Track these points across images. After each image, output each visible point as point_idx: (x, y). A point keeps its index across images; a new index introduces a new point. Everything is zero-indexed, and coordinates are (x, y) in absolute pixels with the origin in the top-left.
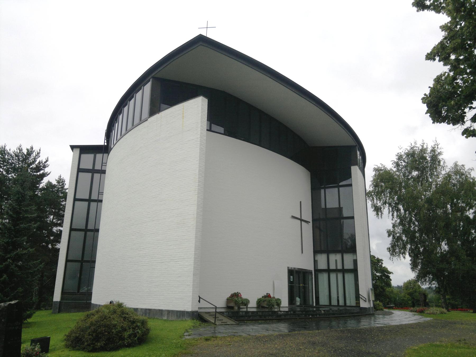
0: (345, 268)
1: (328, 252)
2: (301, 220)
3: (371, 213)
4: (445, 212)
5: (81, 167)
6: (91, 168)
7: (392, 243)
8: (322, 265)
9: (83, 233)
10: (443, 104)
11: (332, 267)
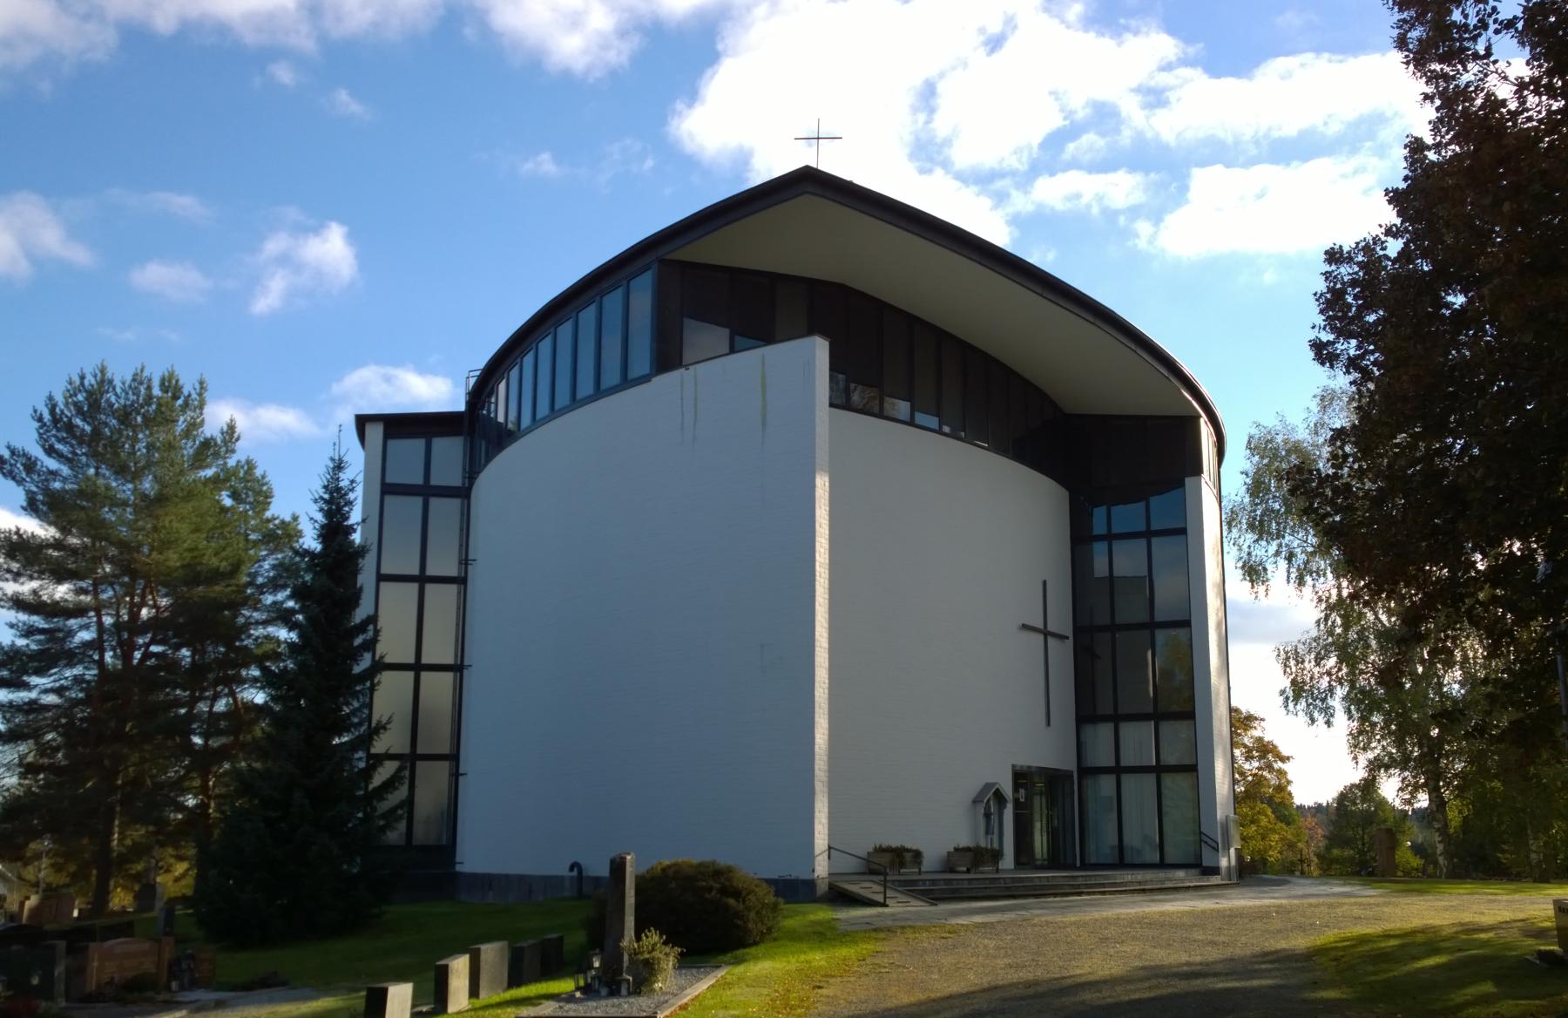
0: (1118, 621)
5: (389, 480)
6: (419, 480)
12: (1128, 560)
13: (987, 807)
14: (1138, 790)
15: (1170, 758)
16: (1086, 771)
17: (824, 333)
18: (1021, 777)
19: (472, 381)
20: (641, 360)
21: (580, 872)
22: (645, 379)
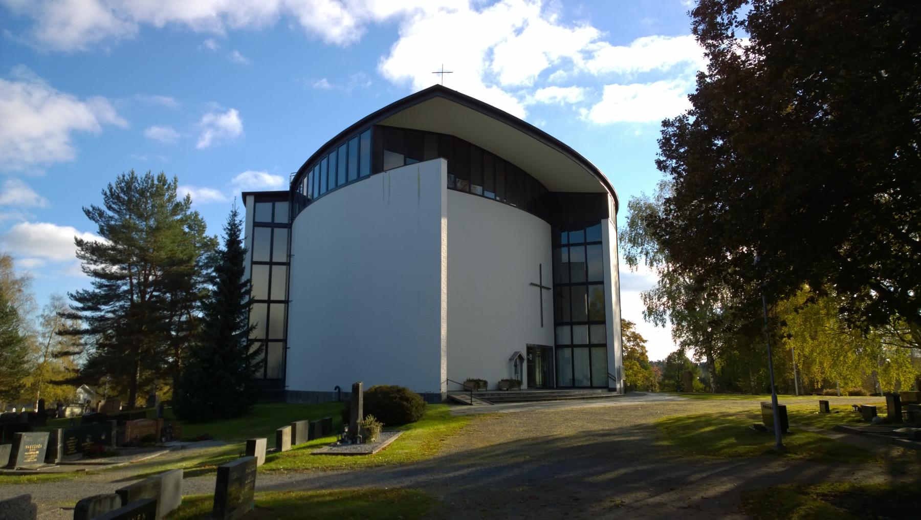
3: (624, 267)
6: (270, 221)
7: (624, 74)
9: (266, 305)
10: (747, 3)
12: (576, 255)
13: (516, 363)
15: (595, 341)
17: (445, 157)
18: (530, 349)
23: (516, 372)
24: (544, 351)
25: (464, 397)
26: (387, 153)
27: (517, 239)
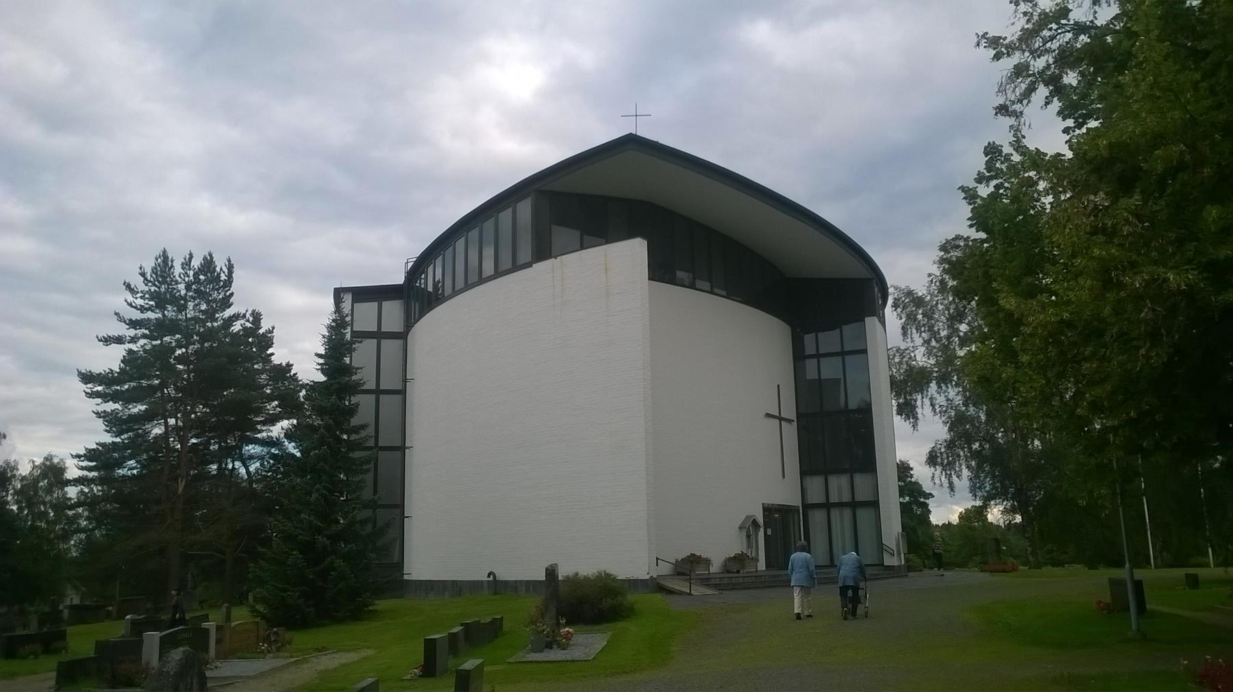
1: (826, 473)
2: (781, 419)
4: (289, 435)
8: (816, 496)
11: (834, 498)
12: (830, 369)
13: (748, 532)
14: (841, 519)
15: (860, 497)
16: (807, 507)
17: (644, 237)
18: (768, 510)
19: (410, 265)
20: (525, 253)
21: (495, 577)
22: (528, 265)
23: (749, 546)
24: (785, 510)
25: (679, 585)
26: (555, 228)
27: (741, 358)
